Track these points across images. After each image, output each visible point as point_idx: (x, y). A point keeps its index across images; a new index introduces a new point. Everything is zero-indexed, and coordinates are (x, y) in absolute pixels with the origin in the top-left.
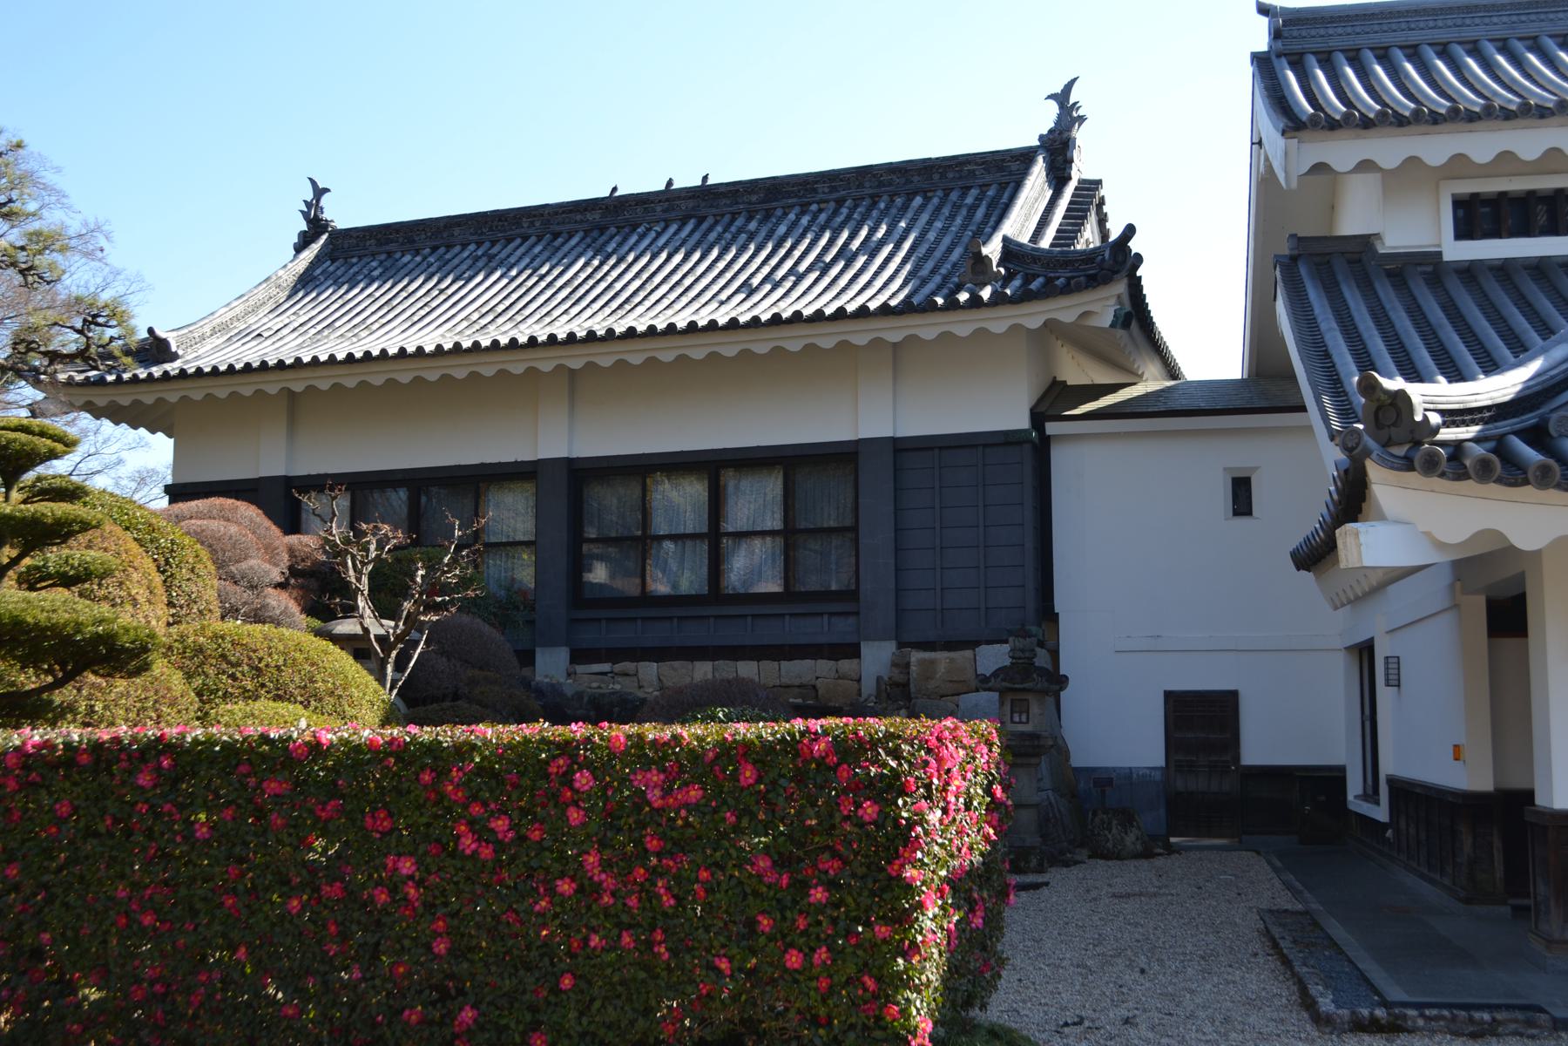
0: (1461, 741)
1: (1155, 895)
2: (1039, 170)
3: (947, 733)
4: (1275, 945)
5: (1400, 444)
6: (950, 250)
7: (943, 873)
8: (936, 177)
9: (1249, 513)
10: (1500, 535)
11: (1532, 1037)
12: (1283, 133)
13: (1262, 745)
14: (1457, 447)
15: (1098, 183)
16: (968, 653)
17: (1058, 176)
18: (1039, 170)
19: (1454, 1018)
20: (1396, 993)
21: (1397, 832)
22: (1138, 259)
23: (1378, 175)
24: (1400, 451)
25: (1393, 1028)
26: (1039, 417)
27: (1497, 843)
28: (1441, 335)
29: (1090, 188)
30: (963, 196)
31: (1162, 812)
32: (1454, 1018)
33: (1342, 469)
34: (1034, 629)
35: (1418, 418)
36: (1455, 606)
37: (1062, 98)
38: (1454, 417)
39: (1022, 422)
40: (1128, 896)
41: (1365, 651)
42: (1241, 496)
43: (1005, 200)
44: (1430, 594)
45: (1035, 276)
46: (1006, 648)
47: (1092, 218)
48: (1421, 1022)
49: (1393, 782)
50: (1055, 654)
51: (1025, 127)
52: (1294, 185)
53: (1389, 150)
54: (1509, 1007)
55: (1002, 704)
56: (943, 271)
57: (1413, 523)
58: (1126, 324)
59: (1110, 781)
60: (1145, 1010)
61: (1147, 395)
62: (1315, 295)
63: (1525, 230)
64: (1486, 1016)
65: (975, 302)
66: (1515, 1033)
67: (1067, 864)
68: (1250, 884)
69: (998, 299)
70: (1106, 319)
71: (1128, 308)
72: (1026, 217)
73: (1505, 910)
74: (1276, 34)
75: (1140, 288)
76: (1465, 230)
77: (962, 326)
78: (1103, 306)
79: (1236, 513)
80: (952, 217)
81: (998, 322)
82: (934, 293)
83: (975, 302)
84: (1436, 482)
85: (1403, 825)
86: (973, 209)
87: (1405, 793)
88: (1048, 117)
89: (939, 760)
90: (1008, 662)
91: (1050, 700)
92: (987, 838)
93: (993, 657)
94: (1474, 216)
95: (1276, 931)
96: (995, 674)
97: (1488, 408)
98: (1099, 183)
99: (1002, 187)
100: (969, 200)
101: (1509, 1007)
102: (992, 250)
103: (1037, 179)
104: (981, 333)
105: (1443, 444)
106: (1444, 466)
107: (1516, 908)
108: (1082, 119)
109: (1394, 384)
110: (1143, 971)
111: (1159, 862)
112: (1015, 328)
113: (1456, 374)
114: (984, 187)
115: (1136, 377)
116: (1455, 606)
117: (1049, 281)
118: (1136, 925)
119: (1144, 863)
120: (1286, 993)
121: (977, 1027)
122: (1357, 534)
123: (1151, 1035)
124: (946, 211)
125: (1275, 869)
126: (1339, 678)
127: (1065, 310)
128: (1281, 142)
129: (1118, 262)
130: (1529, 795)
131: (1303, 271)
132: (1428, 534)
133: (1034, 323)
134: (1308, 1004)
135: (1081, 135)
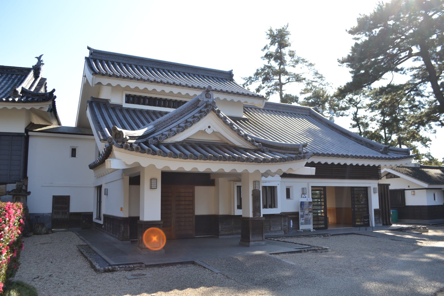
0: (122, 207)
1: (51, 243)
2: (31, 74)
3: (11, 206)
4: (82, 253)
5: (120, 142)
6: (7, 88)
7: (8, 243)
8: (5, 70)
9: (75, 156)
10: (138, 163)
11: (141, 269)
12: (93, 74)
13: (74, 208)
14: (131, 144)
15: (46, 79)
16: (4, 186)
17: (36, 76)
18: (31, 74)
19: (126, 267)
20: (112, 263)
21: (105, 226)
22: (55, 97)
23: (111, 87)
24: (120, 144)
25: (113, 271)
26: (27, 130)
27: (128, 228)
28: (123, 122)
29: (43, 80)
30: (12, 76)
31: (51, 223)
32: (126, 267)
33: (107, 147)
34: (22, 180)
35: (124, 137)
36: (123, 178)
37: (39, 58)
38: (132, 138)
39: (22, 131)
40: (44, 244)
41: (99, 188)
42: (74, 153)
43: (22, 79)
44: (117, 176)
45: (29, 97)
46: (15, 185)
47: (43, 87)
48: (119, 269)
49: (105, 216)
50: (26, 186)
51: (30, 63)
52: (94, 86)
53: (114, 82)
54: (136, 263)
55: (13, 198)
56: (5, 93)
57: (120, 160)
58: (51, 112)
59: (39, 217)
60: (54, 272)
61: (54, 128)
62: (96, 110)
63: (139, 103)
64: (132, 266)
65: (14, 101)
66: (138, 269)
67: (28, 237)
68: (72, 240)
69: (19, 101)
70: (46, 110)
71: (52, 108)
72: (28, 83)
73: (129, 242)
74: (91, 54)
75: (55, 103)
76: (127, 102)
77: (10, 106)
78: (46, 107)
79: (72, 156)
80: (8, 81)
81: (19, 107)
82: (4, 97)
83: (14, 101)
84: (127, 151)
85: (106, 225)
86: (14, 80)
87: (107, 218)
88: (35, 62)
89: (9, 213)
90: (15, 188)
91: (25, 197)
92: (18, 233)
93: (11, 187)
94: (130, 99)
95: (82, 250)
96: (12, 191)
97: (137, 137)
98: (46, 79)
99: (22, 76)
100: (13, 77)
101: (136, 263)
102: (19, 89)
103: (31, 76)
104: (14, 109)
105: (129, 143)
106: (129, 148)
107: (132, 241)
108: (43, 64)
109: (119, 129)
110: (51, 262)
111: (50, 235)
112: (23, 109)
113: (133, 129)
114: (17, 75)
115: (51, 124)
116: (123, 178)
117: (33, 99)
118: (48, 251)
119: (47, 235)
120: (87, 265)
121: (13, 283)
122: (110, 161)
123: (57, 279)
124: (7, 79)
125: (78, 235)
126: (93, 194)
127: (36, 106)
128: (92, 76)
129: (50, 97)
130: (138, 218)
131: (94, 105)
132: (124, 162)
133: (28, 108)
134: (93, 267)
135: (42, 67)
